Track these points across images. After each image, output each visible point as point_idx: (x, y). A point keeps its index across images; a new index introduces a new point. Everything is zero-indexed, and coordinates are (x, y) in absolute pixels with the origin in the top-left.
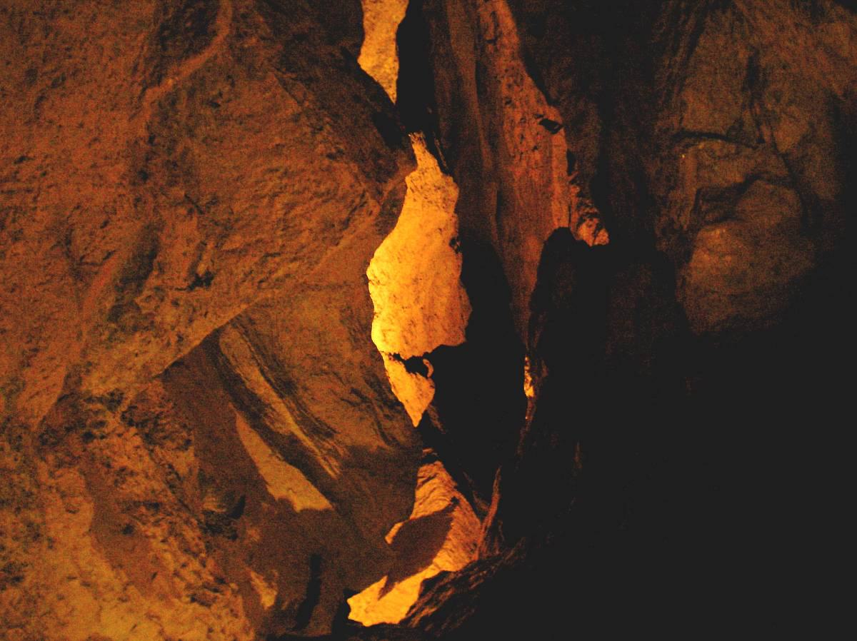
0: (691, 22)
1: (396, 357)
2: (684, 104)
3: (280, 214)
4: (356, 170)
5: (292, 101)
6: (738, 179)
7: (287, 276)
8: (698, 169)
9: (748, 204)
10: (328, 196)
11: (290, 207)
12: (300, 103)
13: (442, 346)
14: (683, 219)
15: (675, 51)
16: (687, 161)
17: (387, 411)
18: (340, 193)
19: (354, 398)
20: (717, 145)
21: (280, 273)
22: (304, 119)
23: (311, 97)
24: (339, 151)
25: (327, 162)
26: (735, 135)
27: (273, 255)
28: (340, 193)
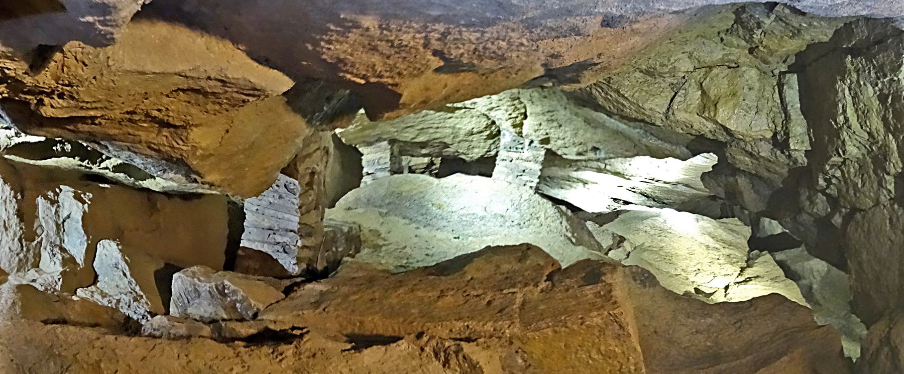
0: (612, 94)
1: (743, 270)
2: (651, 109)
3: (601, 357)
4: (595, 313)
5: (545, 331)
6: (700, 92)
7: (635, 364)
8: (686, 112)
9: (712, 93)
10: (602, 331)
11: (599, 351)
12: (548, 327)
13: (749, 242)
14: (709, 126)
15: (623, 105)
16: (681, 116)
17: (752, 309)
18: (603, 326)
19: (738, 325)
20: (677, 99)
21: (632, 368)
22: (557, 329)
23: (549, 320)
24: (582, 318)
25: (583, 327)
26: (676, 90)
27: (621, 368)
28: (603, 326)
